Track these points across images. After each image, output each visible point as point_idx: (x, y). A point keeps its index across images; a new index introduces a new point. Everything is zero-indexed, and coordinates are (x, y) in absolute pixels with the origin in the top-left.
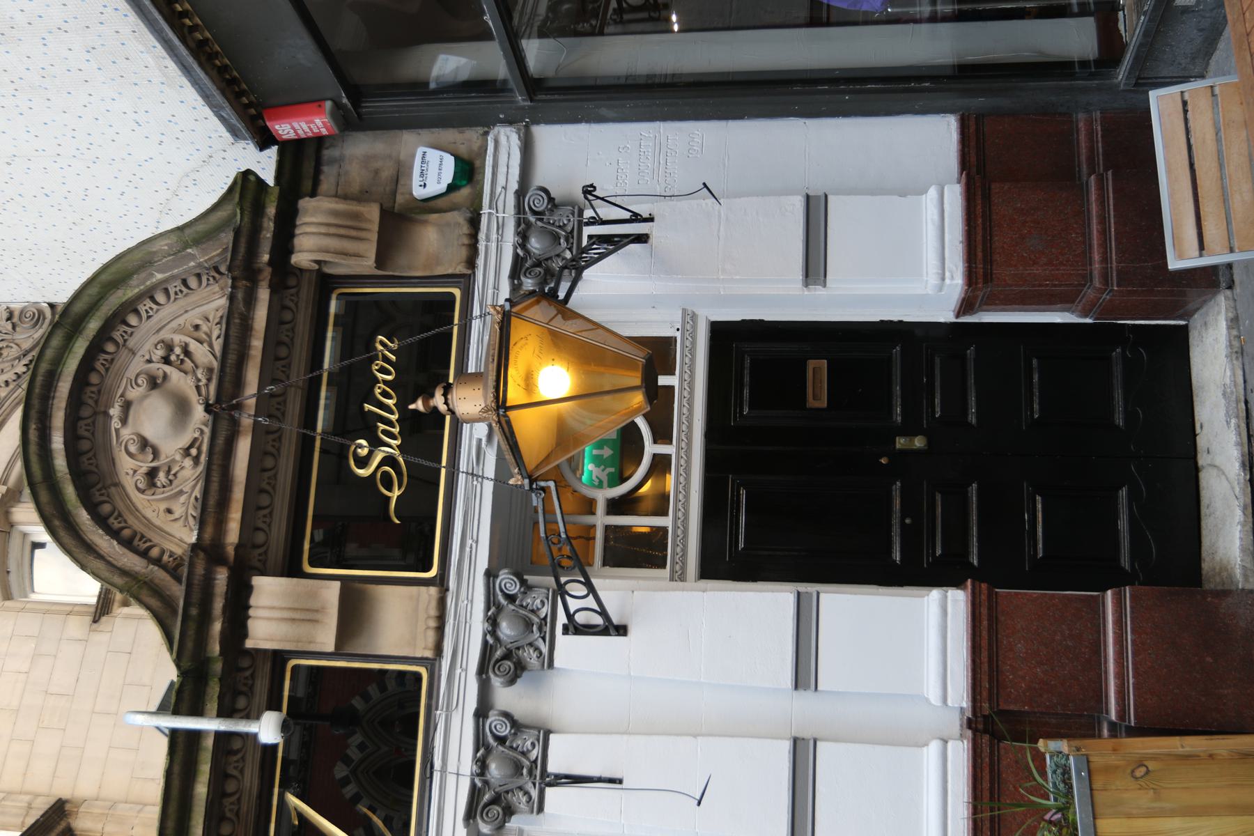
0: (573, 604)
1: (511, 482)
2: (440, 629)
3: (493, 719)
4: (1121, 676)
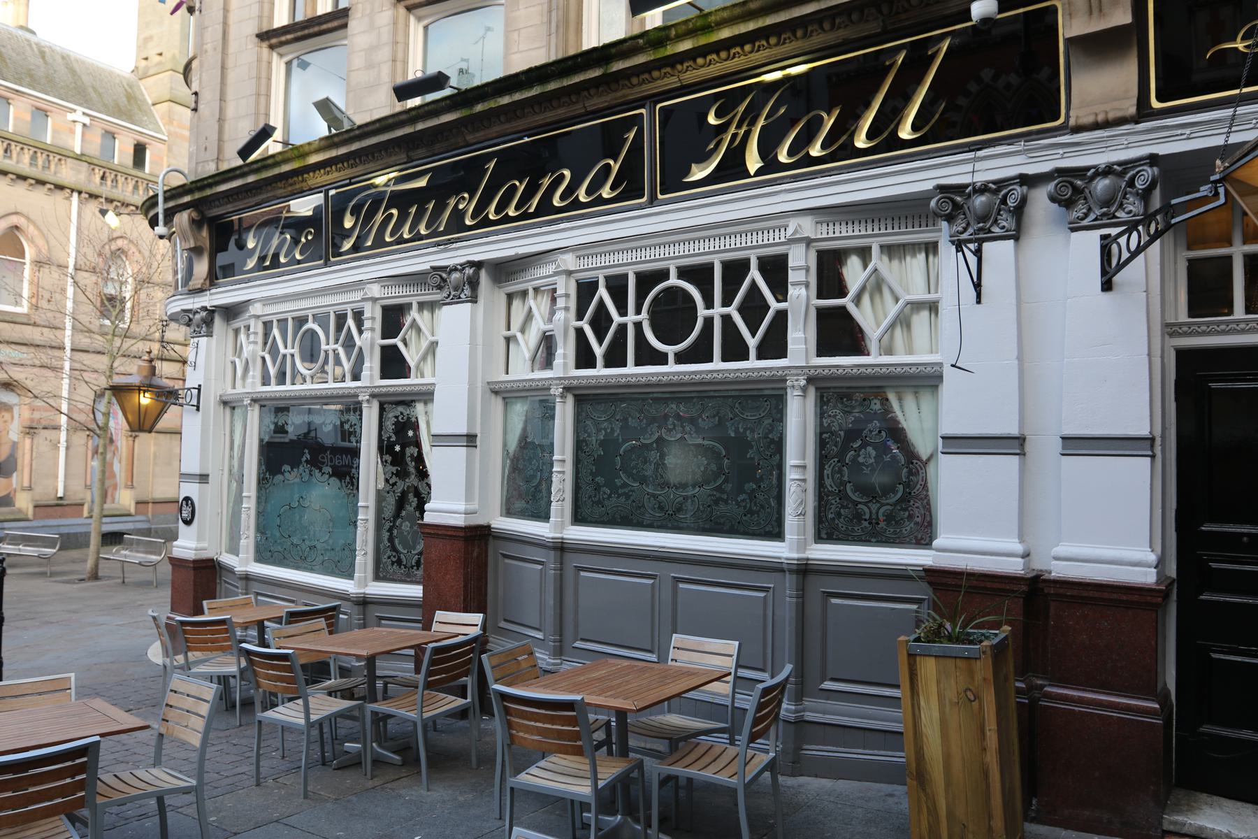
0: (1122, 241)
1: (1218, 162)
2: (1096, 126)
3: (1018, 191)
4: (1081, 701)
